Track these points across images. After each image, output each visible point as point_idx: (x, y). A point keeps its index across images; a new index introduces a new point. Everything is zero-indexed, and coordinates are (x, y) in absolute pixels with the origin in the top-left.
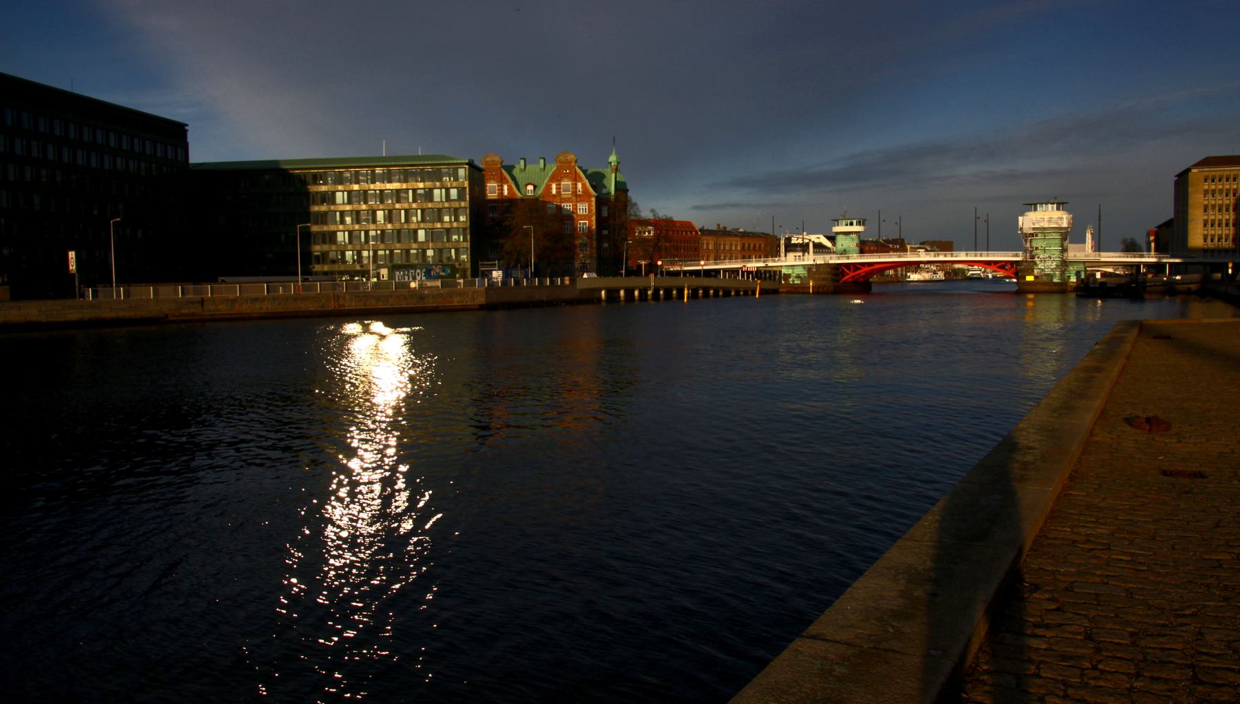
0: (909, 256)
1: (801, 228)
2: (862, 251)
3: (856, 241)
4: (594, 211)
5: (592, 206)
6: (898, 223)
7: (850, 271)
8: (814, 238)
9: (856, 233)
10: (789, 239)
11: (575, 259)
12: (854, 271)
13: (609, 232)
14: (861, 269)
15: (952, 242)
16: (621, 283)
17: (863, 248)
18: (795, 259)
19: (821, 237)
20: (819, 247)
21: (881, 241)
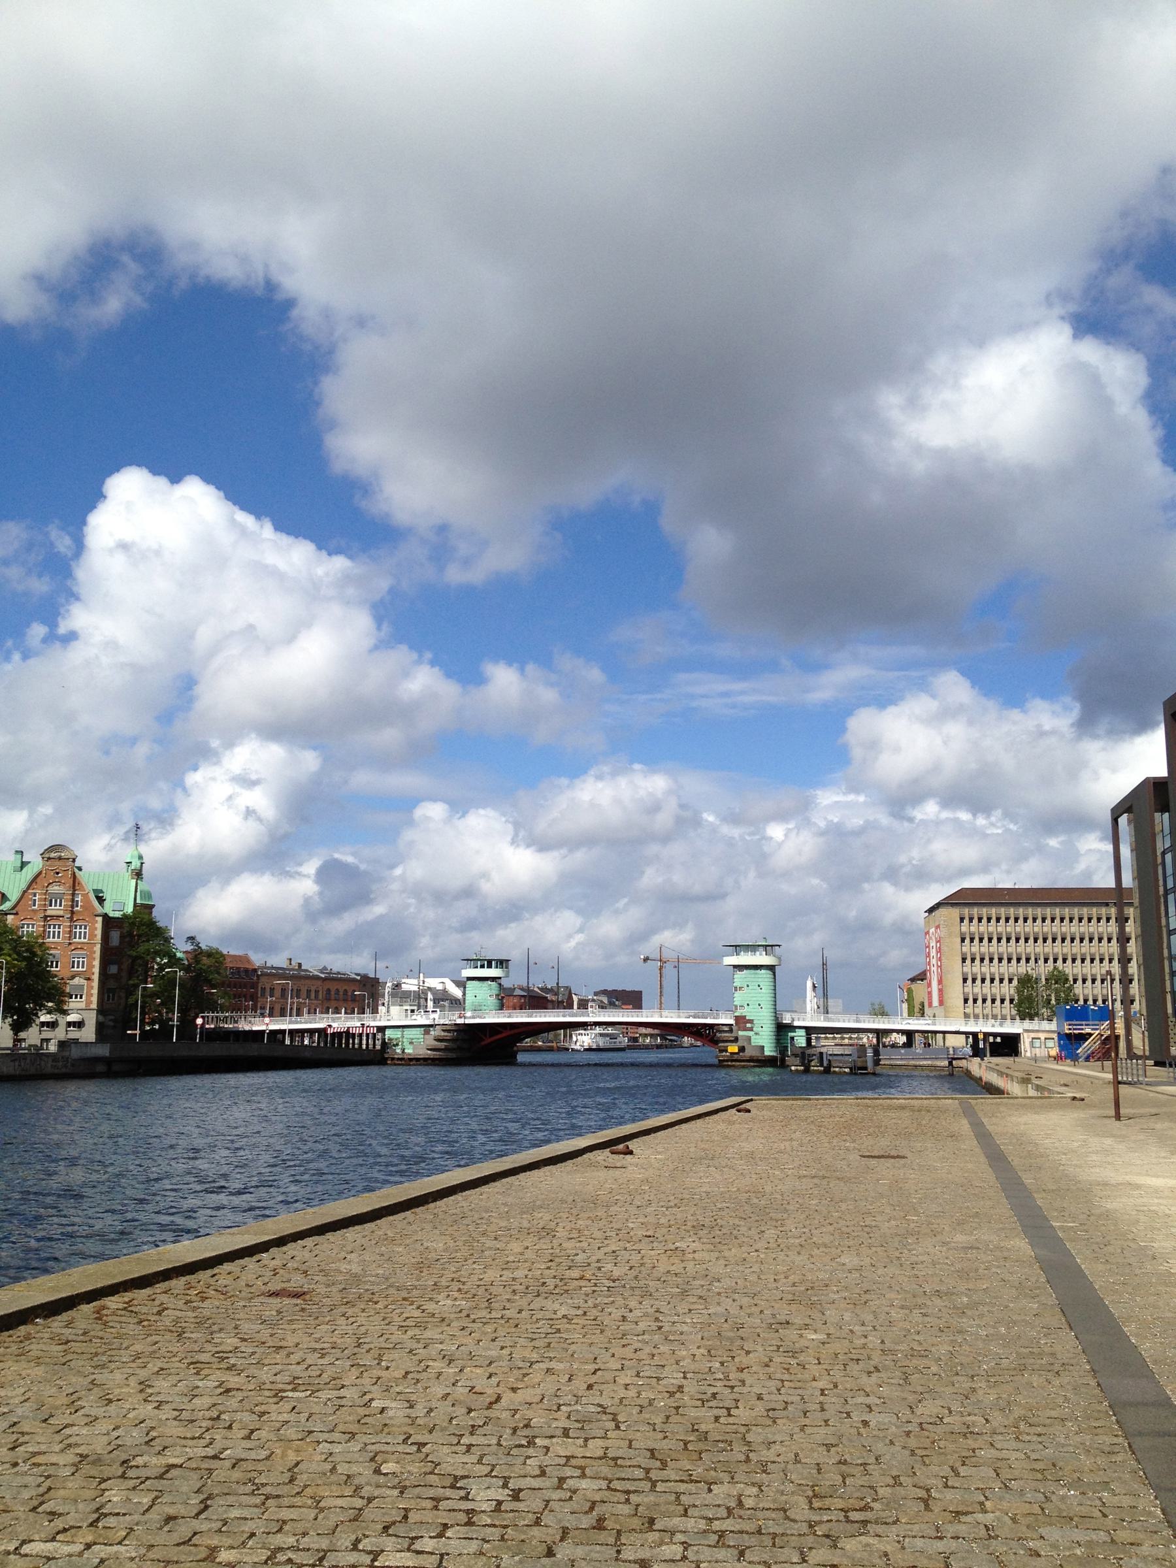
0: (644, 1014)
1: (416, 970)
2: (501, 1007)
3: (495, 991)
4: (99, 937)
5: (96, 929)
6: (556, 967)
7: (486, 1036)
8: (434, 983)
9: (493, 979)
10: (398, 986)
11: (59, 614)
12: (490, 1037)
13: (120, 970)
14: (501, 1032)
15: (641, 992)
16: (799, 1332)
17: (505, 998)
18: (407, 1016)
19: (447, 981)
20: (442, 999)
21: (536, 989)
